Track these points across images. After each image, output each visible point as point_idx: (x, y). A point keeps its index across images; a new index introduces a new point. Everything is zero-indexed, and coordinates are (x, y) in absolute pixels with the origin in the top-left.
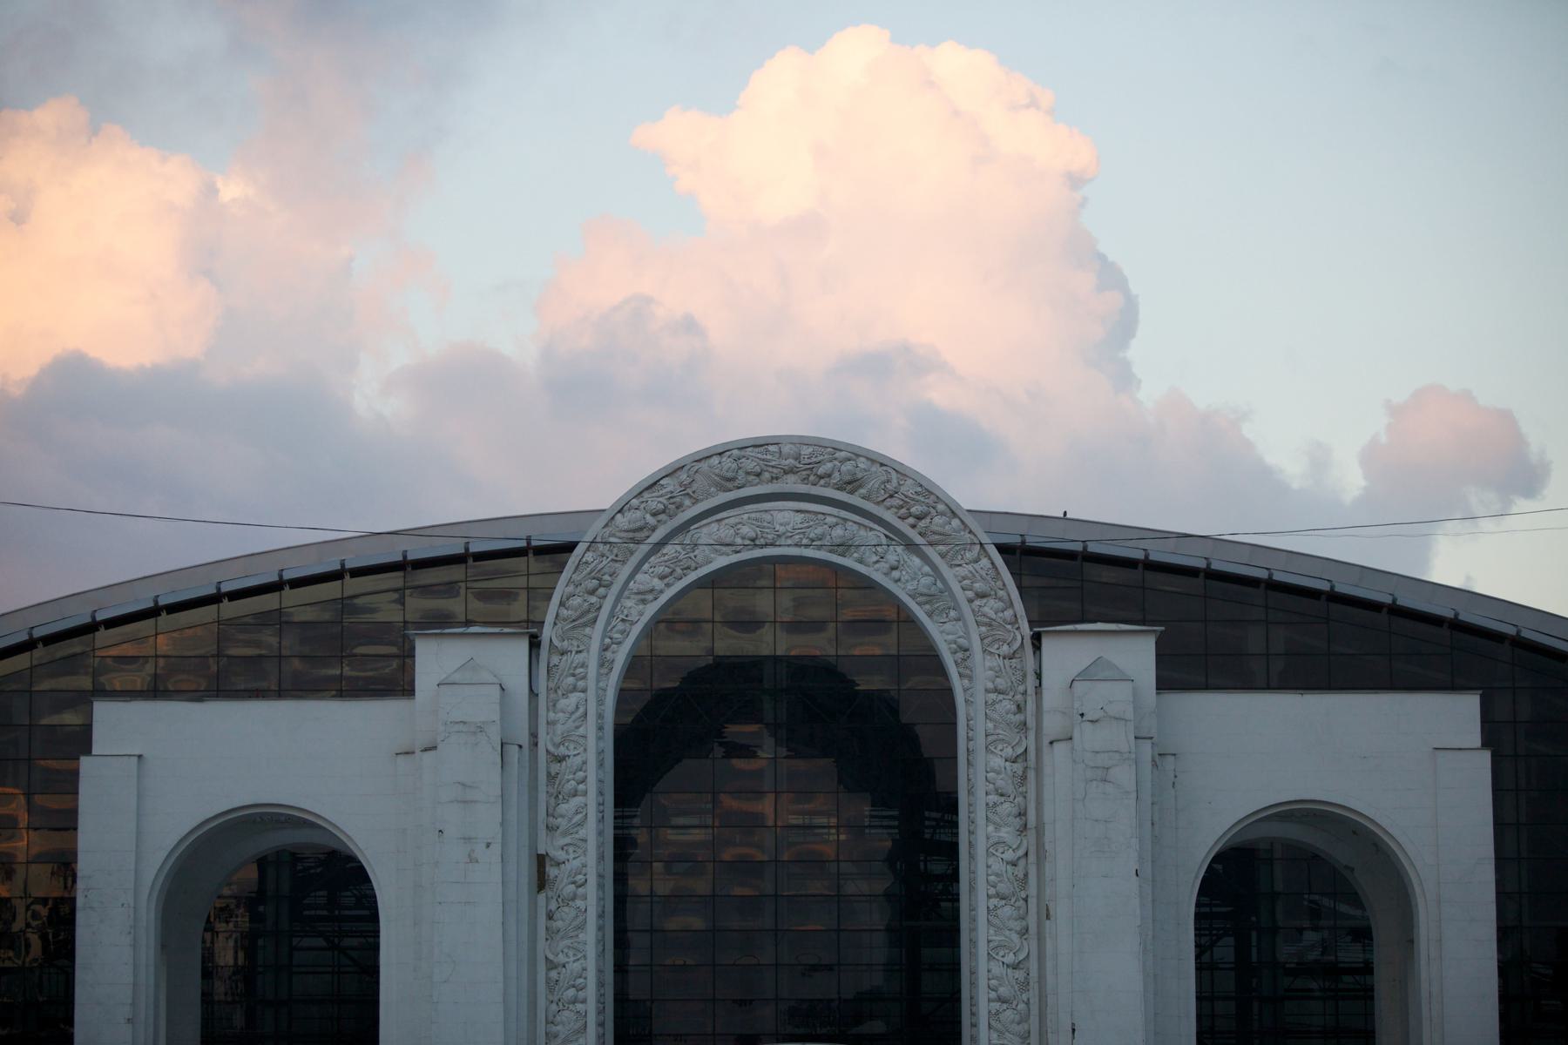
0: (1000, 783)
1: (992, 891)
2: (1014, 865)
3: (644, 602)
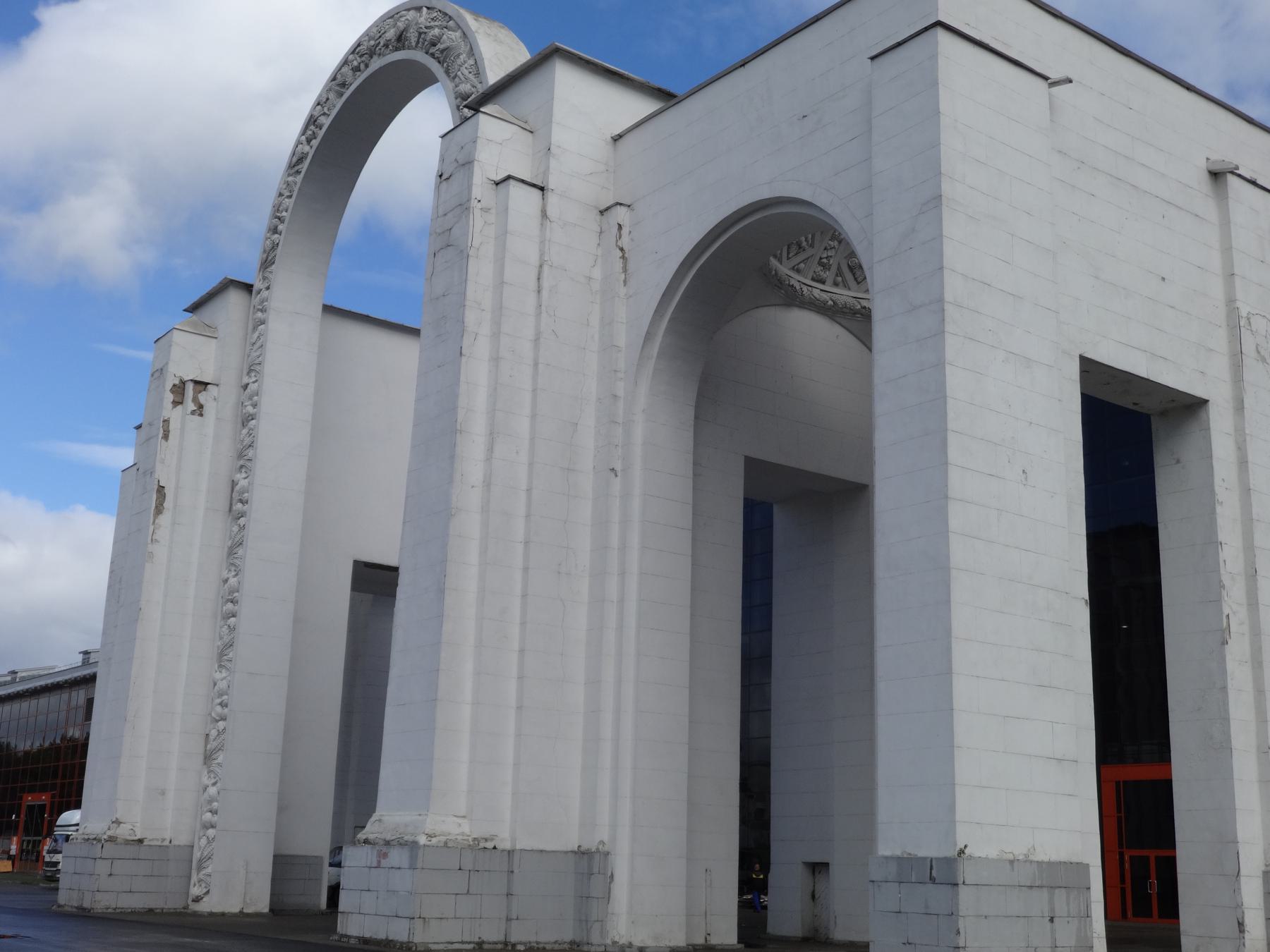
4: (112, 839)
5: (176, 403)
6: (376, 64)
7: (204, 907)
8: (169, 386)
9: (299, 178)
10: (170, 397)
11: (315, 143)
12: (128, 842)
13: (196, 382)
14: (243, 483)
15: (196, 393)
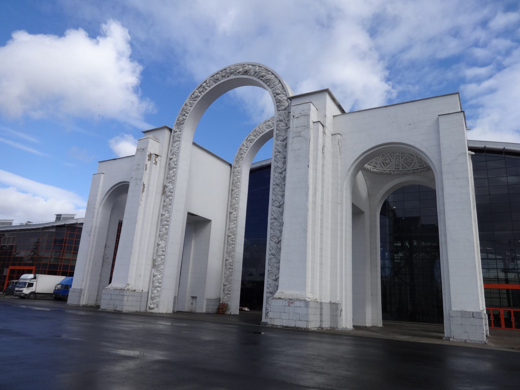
0: (278, 148)
1: (268, 291)
2: (281, 174)
3: (251, 142)
4: (128, 290)
5: (149, 160)
6: (232, 77)
7: (155, 311)
8: (147, 155)
9: (196, 102)
10: (147, 158)
11: (203, 94)
12: (132, 291)
13: (156, 155)
14: (170, 186)
15: (156, 158)
